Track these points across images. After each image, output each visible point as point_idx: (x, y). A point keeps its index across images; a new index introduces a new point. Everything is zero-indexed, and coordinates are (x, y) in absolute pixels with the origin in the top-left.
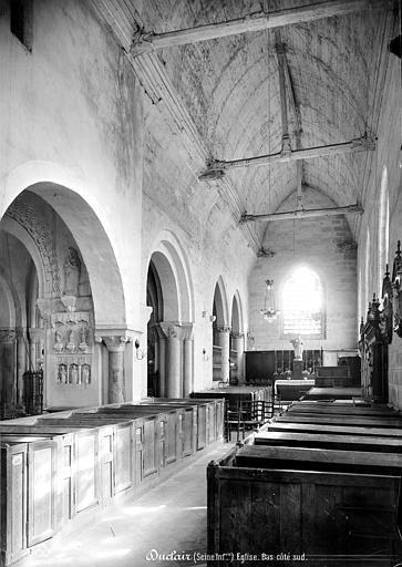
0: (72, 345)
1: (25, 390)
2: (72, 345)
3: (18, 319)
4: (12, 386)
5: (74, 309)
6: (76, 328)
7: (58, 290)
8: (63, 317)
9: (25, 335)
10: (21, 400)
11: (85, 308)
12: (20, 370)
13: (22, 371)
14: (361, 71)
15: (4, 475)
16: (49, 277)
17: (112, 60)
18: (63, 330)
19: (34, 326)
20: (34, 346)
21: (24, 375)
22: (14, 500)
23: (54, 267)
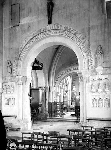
0: (100, 90)
1: (49, 109)
2: (100, 90)
3: (46, 83)
4: (44, 107)
5: (102, 73)
6: (102, 82)
7: (92, 65)
8: (96, 78)
9: (48, 89)
10: (47, 112)
11: (106, 73)
12: (47, 102)
13: (47, 102)
14: (72, 43)
15: (70, 149)
16: (86, 60)
17: (29, 35)
18: (95, 83)
19: (51, 86)
20: (51, 93)
21: (48, 103)
22: (12, 132)
23: (89, 56)
